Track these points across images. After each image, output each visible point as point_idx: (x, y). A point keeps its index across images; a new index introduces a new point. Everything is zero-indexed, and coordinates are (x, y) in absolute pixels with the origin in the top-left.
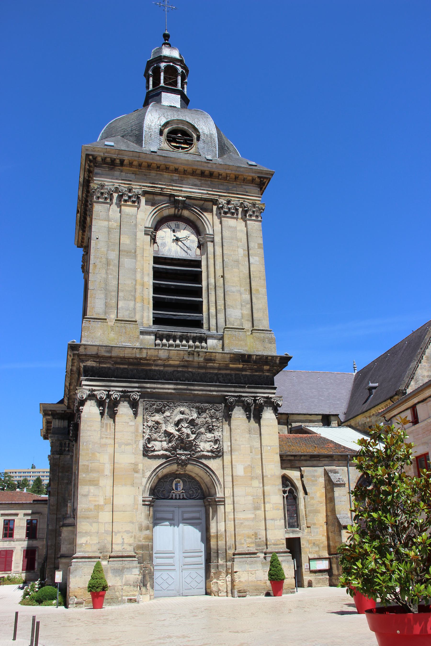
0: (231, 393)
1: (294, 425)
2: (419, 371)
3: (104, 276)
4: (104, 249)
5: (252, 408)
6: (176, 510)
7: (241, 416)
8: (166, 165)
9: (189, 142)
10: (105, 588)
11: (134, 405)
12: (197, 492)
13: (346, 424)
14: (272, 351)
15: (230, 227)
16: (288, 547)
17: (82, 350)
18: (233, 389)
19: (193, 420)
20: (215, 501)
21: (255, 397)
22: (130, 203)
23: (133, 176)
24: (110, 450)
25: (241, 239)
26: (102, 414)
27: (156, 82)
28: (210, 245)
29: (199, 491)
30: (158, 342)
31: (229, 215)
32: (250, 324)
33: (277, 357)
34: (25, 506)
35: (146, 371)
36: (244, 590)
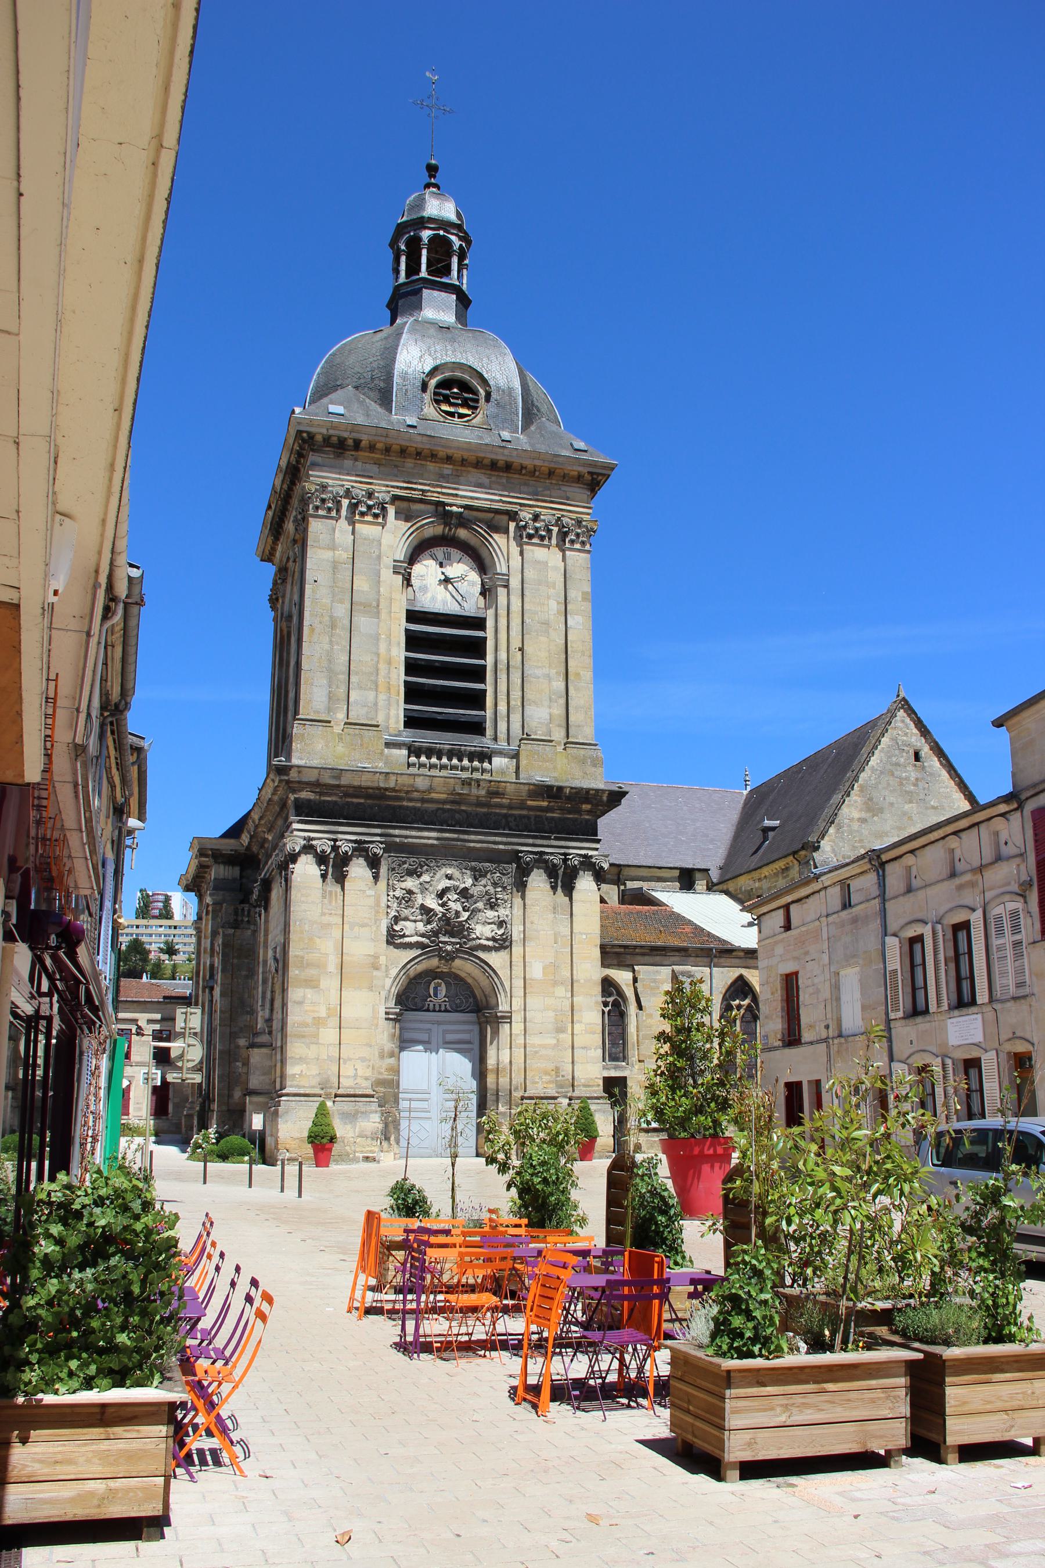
0: (527, 847)
1: (630, 885)
2: (845, 810)
3: (327, 647)
4: (326, 601)
5: (561, 872)
6: (435, 1028)
7: (542, 885)
8: (431, 450)
9: (472, 404)
10: (332, 1139)
11: (374, 863)
12: (467, 1002)
13: (720, 887)
14: (597, 781)
15: (538, 562)
16: (605, 1091)
17: (293, 775)
18: (531, 841)
19: (466, 889)
20: (497, 1016)
21: (565, 854)
22: (369, 518)
23: (375, 468)
24: (337, 933)
26: (324, 877)
27: (413, 268)
28: (502, 592)
29: (471, 1000)
30: (413, 759)
31: (535, 540)
32: (563, 732)
33: (603, 791)
34: (148, 1005)
35: (394, 808)
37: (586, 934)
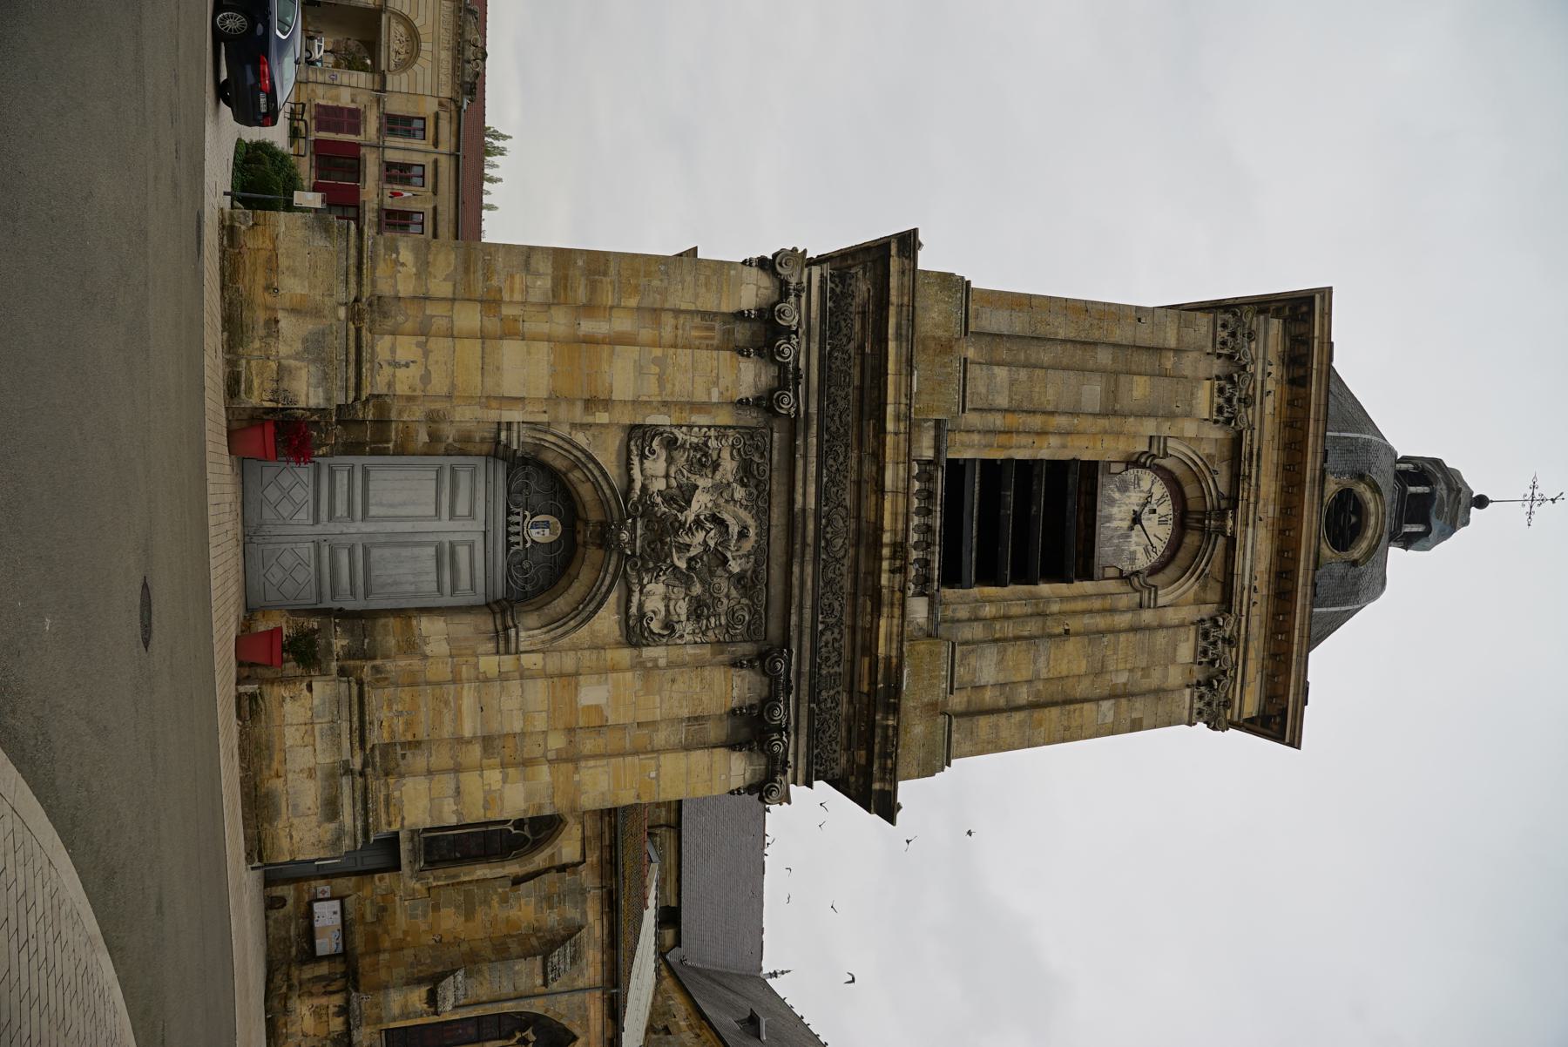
11: (765, 403)
19: (725, 561)
25: (1148, 676)
36: (258, 713)
37: (658, 777)
